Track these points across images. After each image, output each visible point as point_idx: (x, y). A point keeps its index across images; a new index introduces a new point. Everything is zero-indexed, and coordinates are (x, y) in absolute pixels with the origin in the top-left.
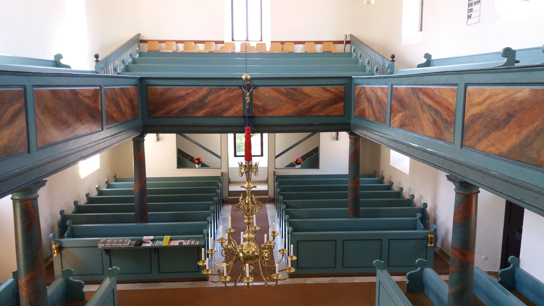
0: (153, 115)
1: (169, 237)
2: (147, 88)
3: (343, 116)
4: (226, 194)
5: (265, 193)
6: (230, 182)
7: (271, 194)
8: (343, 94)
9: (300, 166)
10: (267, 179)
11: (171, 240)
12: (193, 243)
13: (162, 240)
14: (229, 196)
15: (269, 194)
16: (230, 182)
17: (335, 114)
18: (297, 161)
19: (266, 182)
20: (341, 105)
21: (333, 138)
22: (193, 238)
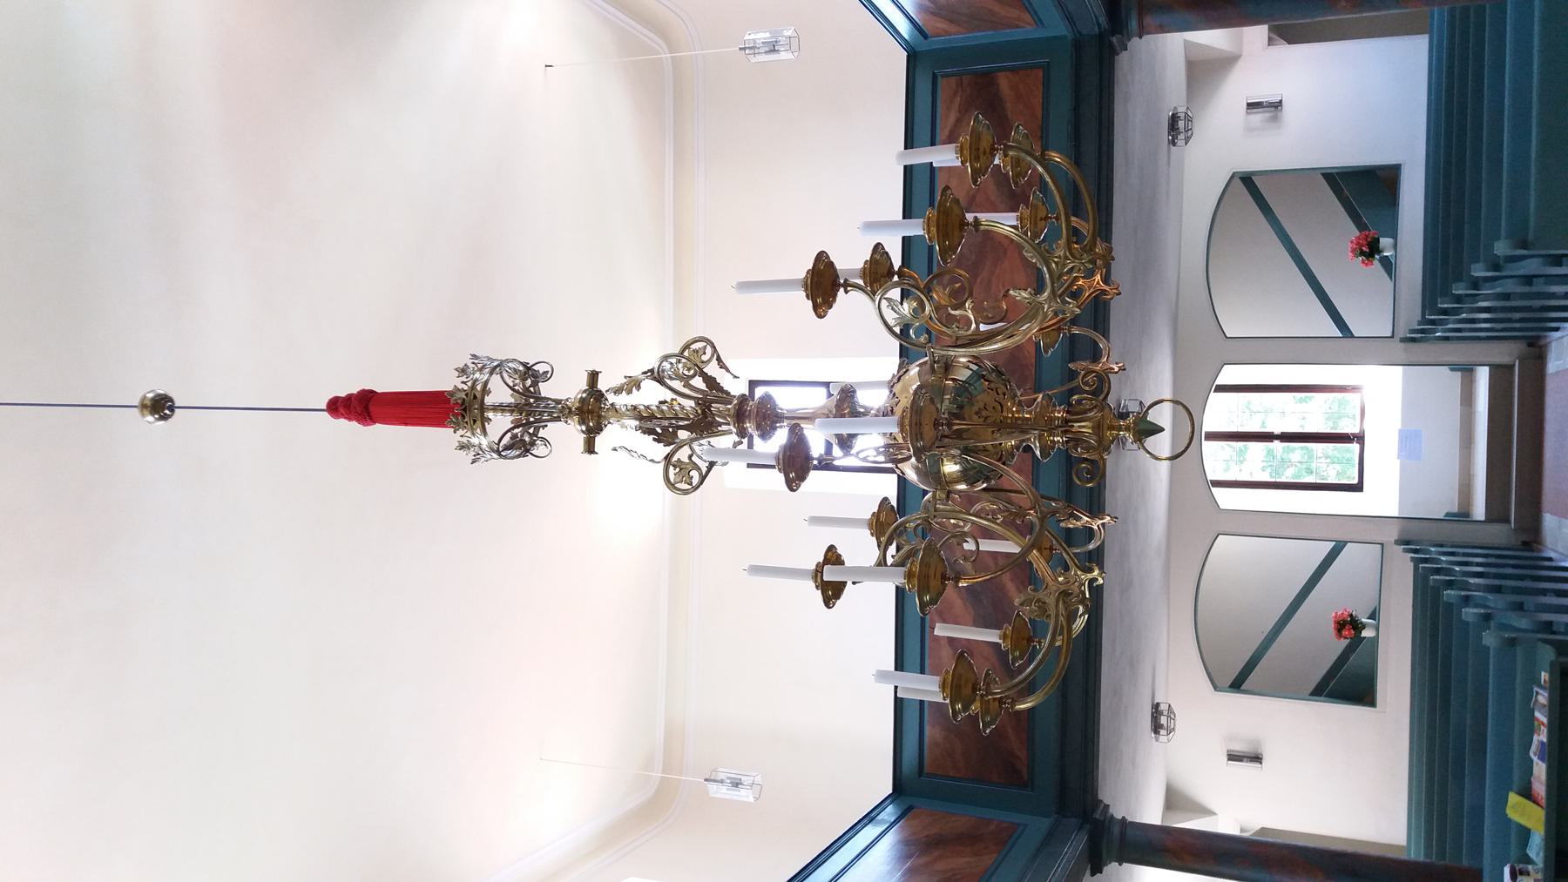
0: (1025, 771)
1: (1513, 798)
2: (929, 775)
3: (1047, 69)
4: (1499, 534)
5: (1500, 375)
6: (1463, 516)
7: (1505, 353)
8: (966, 80)
9: (1385, 242)
10: (1454, 367)
11: (1527, 793)
12: (1543, 698)
13: (1525, 834)
14: (1507, 521)
15: (1505, 360)
16: (1463, 516)
17: (1037, 101)
18: (1362, 253)
19: (1467, 370)
20: (1004, 83)
21: (1275, 119)
22: (1529, 696)
